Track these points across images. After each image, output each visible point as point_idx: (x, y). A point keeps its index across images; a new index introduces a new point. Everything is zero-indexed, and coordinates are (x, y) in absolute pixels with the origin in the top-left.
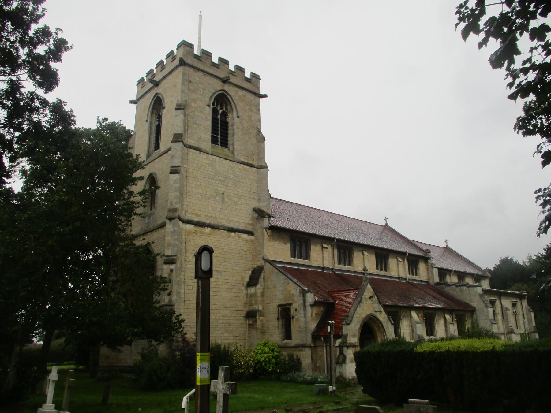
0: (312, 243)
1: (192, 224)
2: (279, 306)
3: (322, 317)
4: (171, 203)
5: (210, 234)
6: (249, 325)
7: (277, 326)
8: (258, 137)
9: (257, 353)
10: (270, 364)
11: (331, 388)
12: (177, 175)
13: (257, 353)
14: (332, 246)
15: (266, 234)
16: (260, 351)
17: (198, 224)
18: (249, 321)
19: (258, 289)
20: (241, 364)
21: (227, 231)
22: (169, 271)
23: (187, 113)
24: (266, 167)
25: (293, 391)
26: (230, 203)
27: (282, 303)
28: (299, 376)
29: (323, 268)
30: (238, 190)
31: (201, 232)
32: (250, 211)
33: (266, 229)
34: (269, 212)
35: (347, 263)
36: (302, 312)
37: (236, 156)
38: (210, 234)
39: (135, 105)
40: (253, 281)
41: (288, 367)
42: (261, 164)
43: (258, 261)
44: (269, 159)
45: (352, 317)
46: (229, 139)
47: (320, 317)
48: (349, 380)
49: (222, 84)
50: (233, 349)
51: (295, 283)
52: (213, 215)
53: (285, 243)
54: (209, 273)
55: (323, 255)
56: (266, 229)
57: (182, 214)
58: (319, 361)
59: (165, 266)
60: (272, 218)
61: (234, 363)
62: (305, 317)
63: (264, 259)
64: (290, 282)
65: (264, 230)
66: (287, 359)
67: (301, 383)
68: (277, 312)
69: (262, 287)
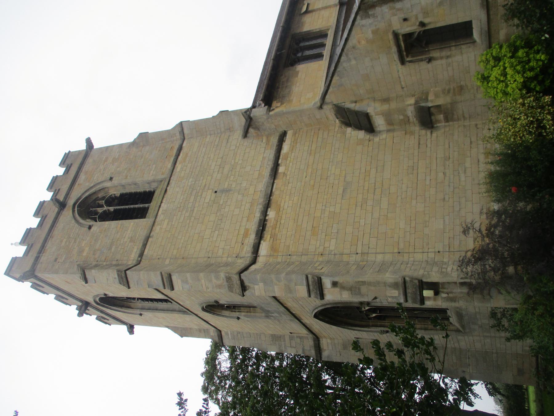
0: (298, 31)
1: (259, 243)
2: (403, 62)
4: (219, 286)
5: (278, 211)
6: (447, 120)
7: (444, 61)
8: (141, 144)
9: (505, 94)
10: (529, 61)
12: (174, 278)
13: (505, 94)
15: (278, 108)
16: (501, 86)
17: (260, 235)
18: (439, 122)
19: (373, 109)
20: (532, 122)
21: (274, 179)
22: (337, 290)
23: (94, 263)
24: (181, 123)
27: (396, 57)
30: (213, 167)
31: (274, 227)
32: (246, 142)
33: (269, 110)
37: (163, 177)
38: (278, 211)
39: (135, 326)
40: (361, 122)
42: (178, 134)
44: (167, 123)
46: (143, 191)
49: (66, 209)
50: (497, 146)
52: (248, 206)
53: (297, 73)
55: (319, 9)
56: (269, 110)
57: (241, 263)
61: (530, 139)
63: (321, 107)
65: (271, 113)
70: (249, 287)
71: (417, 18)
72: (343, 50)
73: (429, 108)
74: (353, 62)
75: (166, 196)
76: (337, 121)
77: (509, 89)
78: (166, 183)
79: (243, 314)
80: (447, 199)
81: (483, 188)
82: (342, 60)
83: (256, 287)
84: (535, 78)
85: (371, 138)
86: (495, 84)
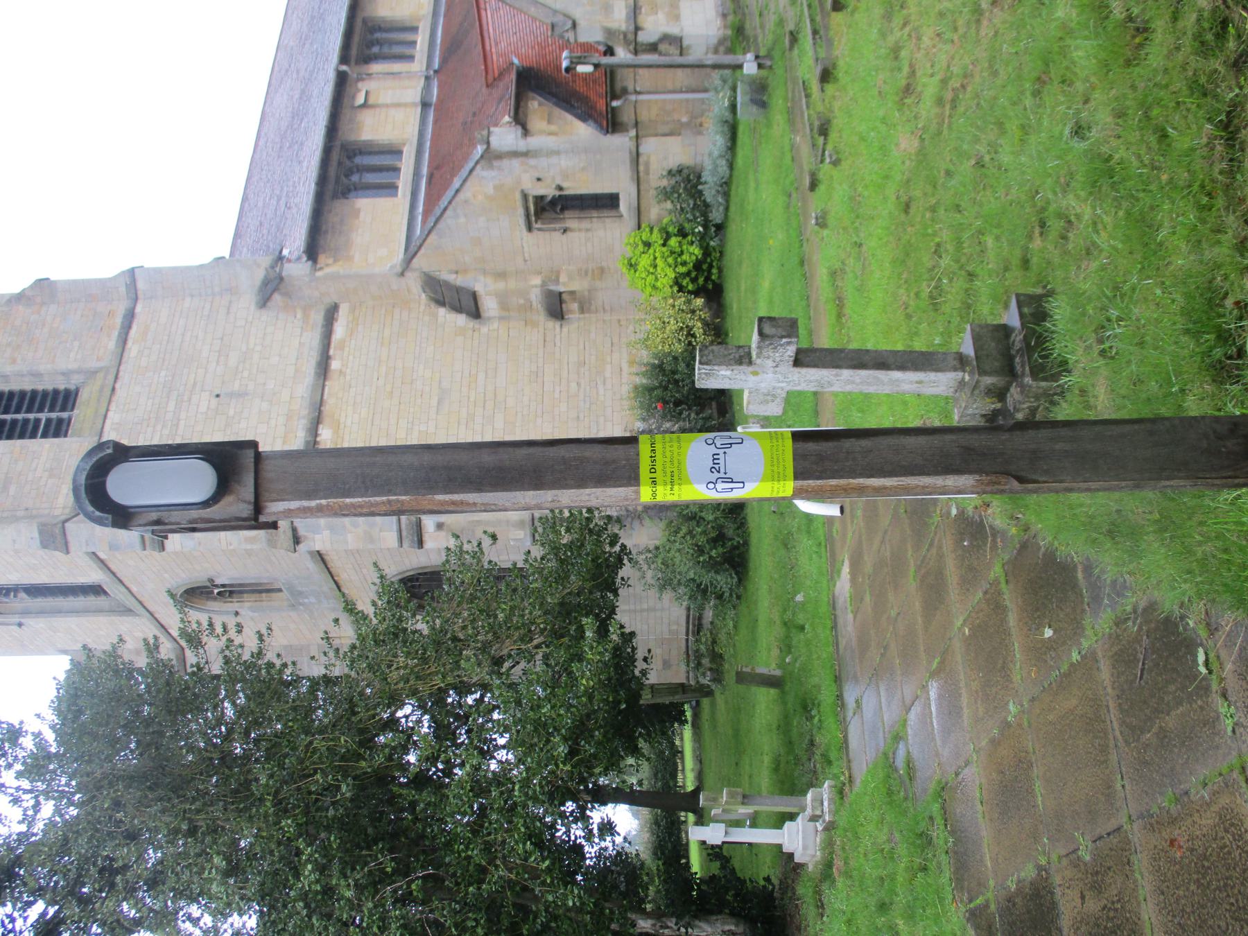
0: (352, 138)
2: (530, 229)
3: (557, 105)
7: (583, 235)
8: (38, 300)
9: (654, 287)
10: (682, 253)
11: (750, 68)
13: (654, 287)
14: (362, 80)
15: (330, 267)
16: (650, 278)
18: (571, 312)
19: (483, 286)
21: (325, 379)
24: (132, 272)
25: (752, 184)
26: (246, 374)
27: (521, 221)
28: (715, 170)
29: (425, 105)
32: (266, 315)
34: (266, 261)
35: (408, 37)
36: (543, 162)
41: (691, 202)
42: (123, 289)
43: (409, 291)
44: (104, 265)
45: (555, 12)
47: (558, 112)
48: (725, 27)
50: (645, 353)
51: (465, 181)
54: (229, 461)
55: (387, 106)
58: (676, 117)
59: (429, 544)
60: (285, 252)
62: (558, 153)
63: (402, 274)
64: (461, 196)
65: (319, 274)
66: (669, 205)
67: (731, 166)
68: (547, 234)
69: (482, 278)
70: (306, 537)
71: (553, 179)
72: (450, 203)
73: (560, 294)
74: (462, 220)
75: (115, 399)
76: (423, 295)
77: (658, 284)
78: (111, 378)
79: (247, 604)
80: (581, 416)
81: (626, 404)
82: (446, 215)
83: (317, 537)
84: (688, 274)
85: (477, 326)
86: (643, 275)
